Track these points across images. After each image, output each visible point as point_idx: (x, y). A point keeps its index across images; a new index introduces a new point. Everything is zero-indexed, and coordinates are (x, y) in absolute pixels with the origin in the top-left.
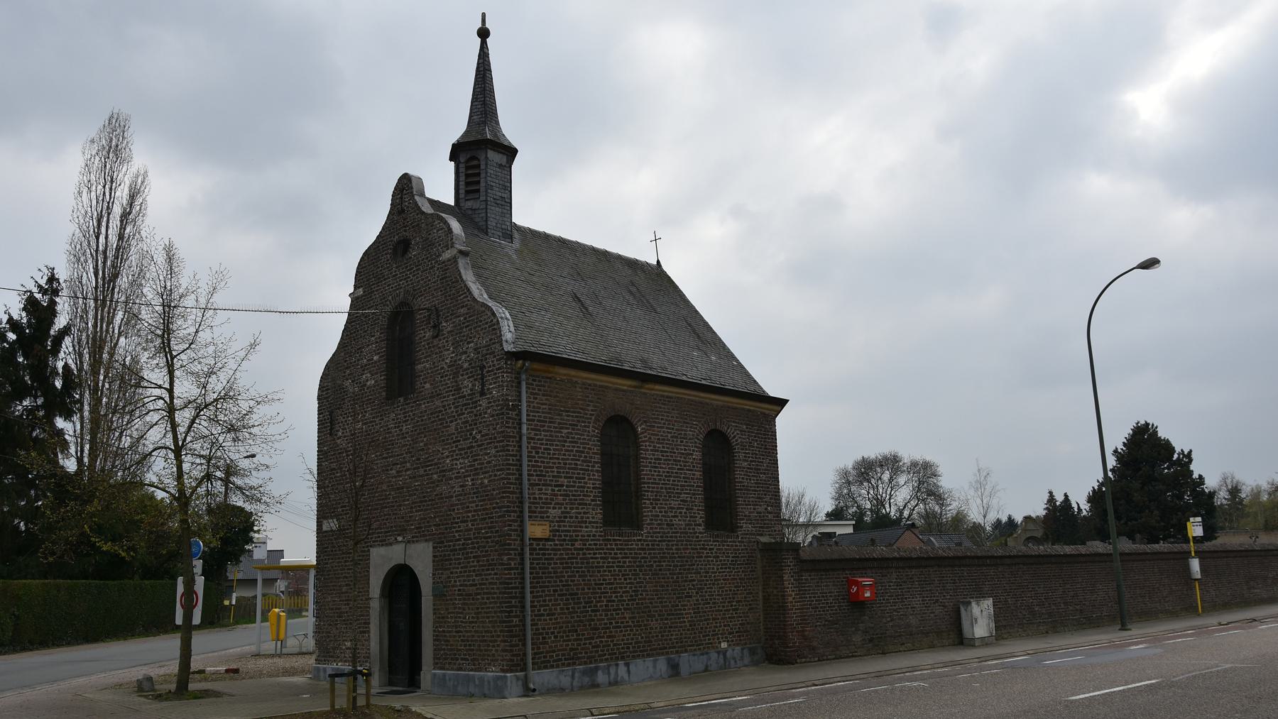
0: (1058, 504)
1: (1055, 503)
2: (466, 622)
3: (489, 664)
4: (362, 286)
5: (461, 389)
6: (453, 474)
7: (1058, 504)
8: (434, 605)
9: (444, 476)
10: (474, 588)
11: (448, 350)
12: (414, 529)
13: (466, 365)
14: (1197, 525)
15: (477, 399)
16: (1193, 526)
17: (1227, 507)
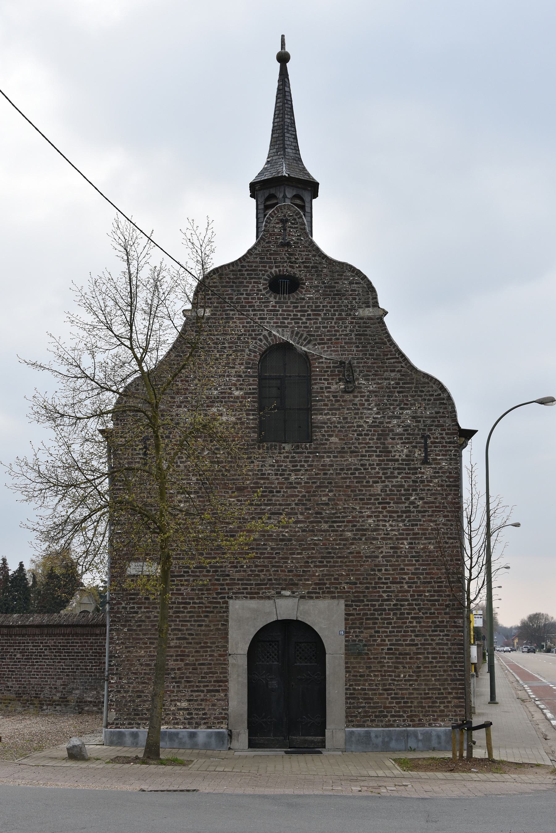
0: (10, 573)
1: (7, 572)
2: (401, 680)
3: (435, 720)
4: (210, 307)
5: (390, 452)
6: (380, 535)
7: (10, 573)
8: (346, 663)
9: (365, 535)
10: (414, 648)
11: (371, 409)
12: (311, 585)
13: (399, 430)
14: (478, 618)
15: (417, 466)
16: (475, 618)
17: (102, 589)
